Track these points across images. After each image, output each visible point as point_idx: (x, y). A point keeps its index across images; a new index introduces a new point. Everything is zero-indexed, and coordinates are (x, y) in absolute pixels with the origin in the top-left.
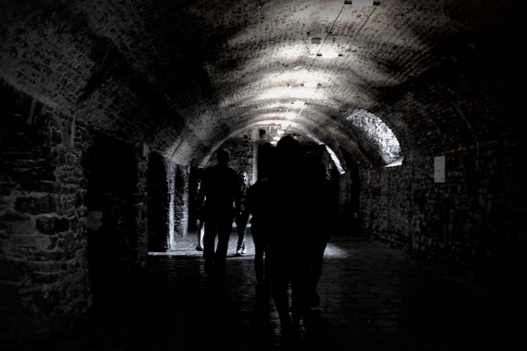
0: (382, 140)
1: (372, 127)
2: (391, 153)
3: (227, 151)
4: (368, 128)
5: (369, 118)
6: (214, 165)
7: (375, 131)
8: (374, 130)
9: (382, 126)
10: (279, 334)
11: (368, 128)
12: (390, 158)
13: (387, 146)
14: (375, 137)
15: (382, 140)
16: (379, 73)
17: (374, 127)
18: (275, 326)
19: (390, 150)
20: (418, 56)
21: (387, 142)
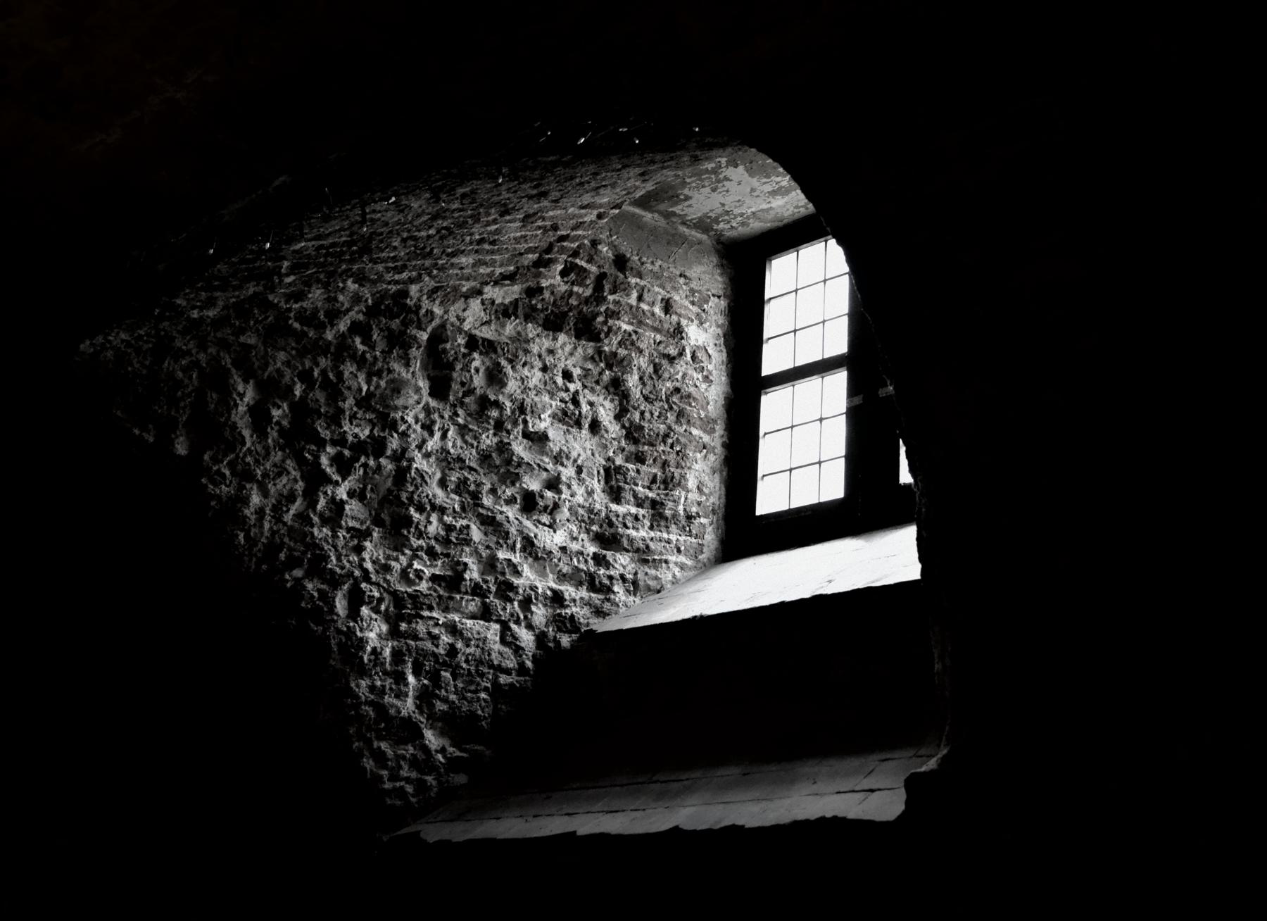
0: (356, 598)
1: (281, 471)
2: (433, 718)
3: (419, 370)
4: (245, 476)
5: (271, 390)
6: (859, 296)
7: (303, 518)
8: (291, 498)
9: (365, 479)
10: (402, 531)
11: (245, 476)
12: (424, 762)
13: (397, 656)
14: (293, 563)
15: (356, 598)
16: (603, 492)
17: (293, 480)
18: (323, 608)
19: (425, 698)
20: (665, 164)
21: (401, 617)
